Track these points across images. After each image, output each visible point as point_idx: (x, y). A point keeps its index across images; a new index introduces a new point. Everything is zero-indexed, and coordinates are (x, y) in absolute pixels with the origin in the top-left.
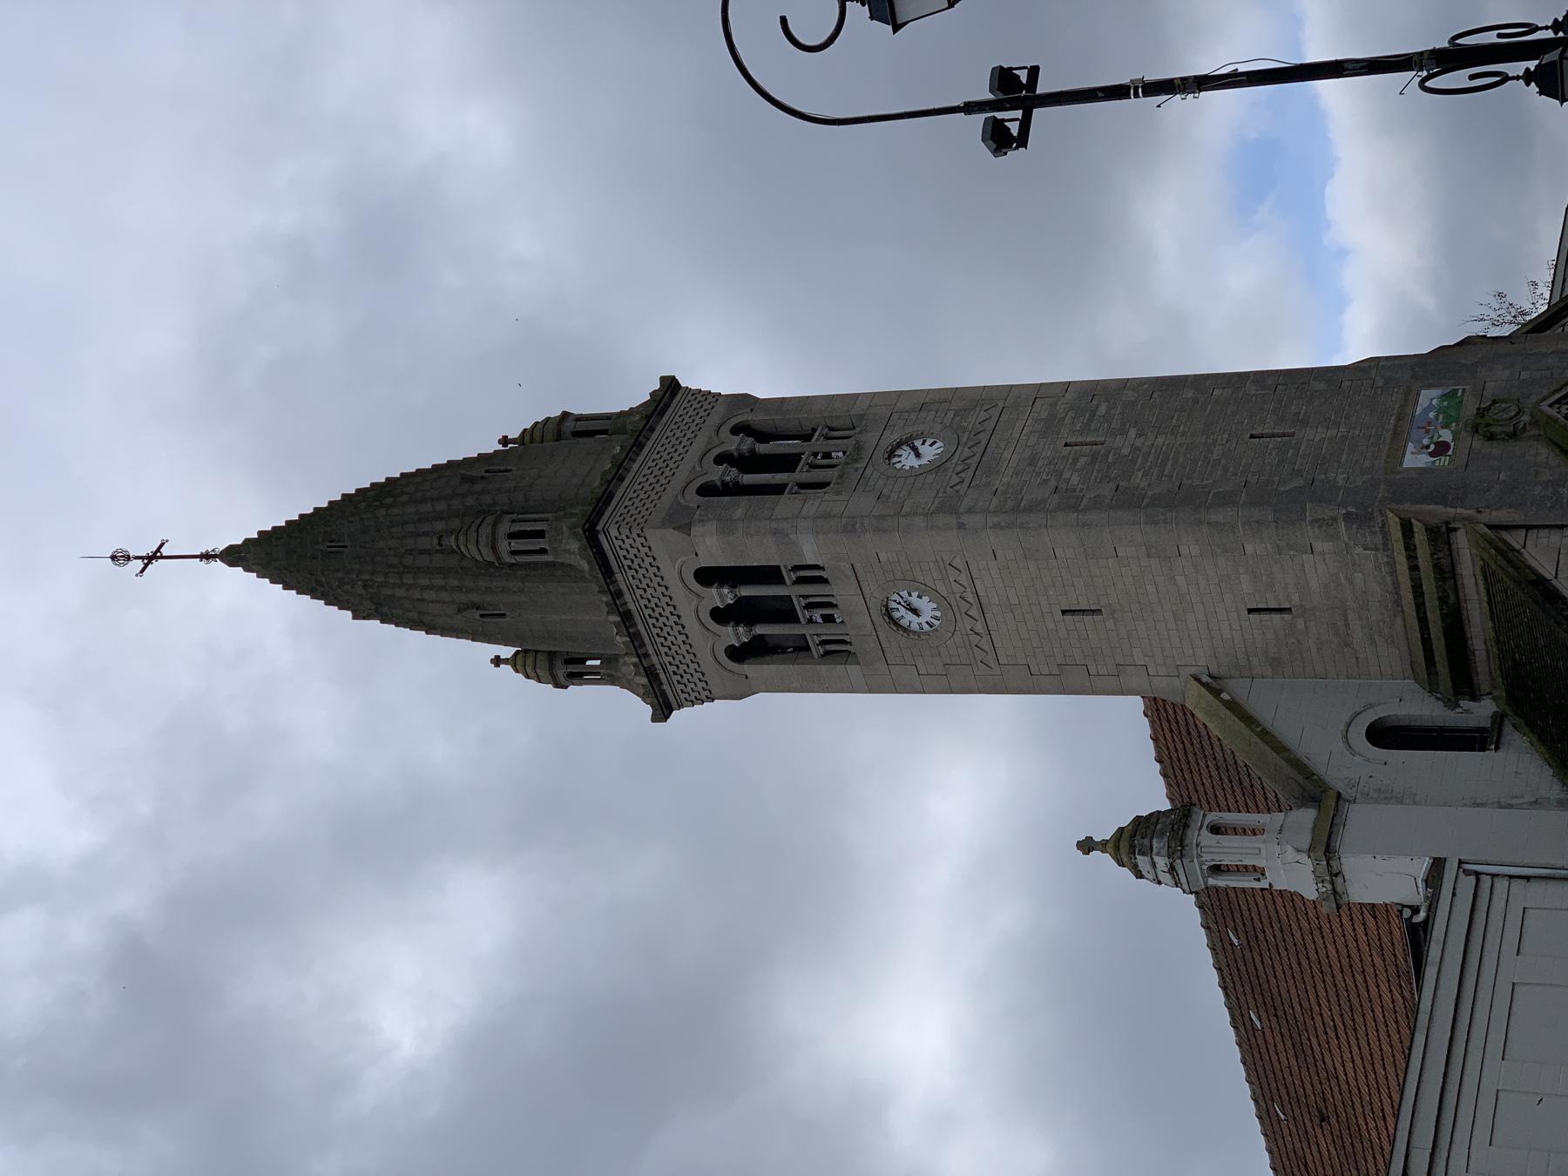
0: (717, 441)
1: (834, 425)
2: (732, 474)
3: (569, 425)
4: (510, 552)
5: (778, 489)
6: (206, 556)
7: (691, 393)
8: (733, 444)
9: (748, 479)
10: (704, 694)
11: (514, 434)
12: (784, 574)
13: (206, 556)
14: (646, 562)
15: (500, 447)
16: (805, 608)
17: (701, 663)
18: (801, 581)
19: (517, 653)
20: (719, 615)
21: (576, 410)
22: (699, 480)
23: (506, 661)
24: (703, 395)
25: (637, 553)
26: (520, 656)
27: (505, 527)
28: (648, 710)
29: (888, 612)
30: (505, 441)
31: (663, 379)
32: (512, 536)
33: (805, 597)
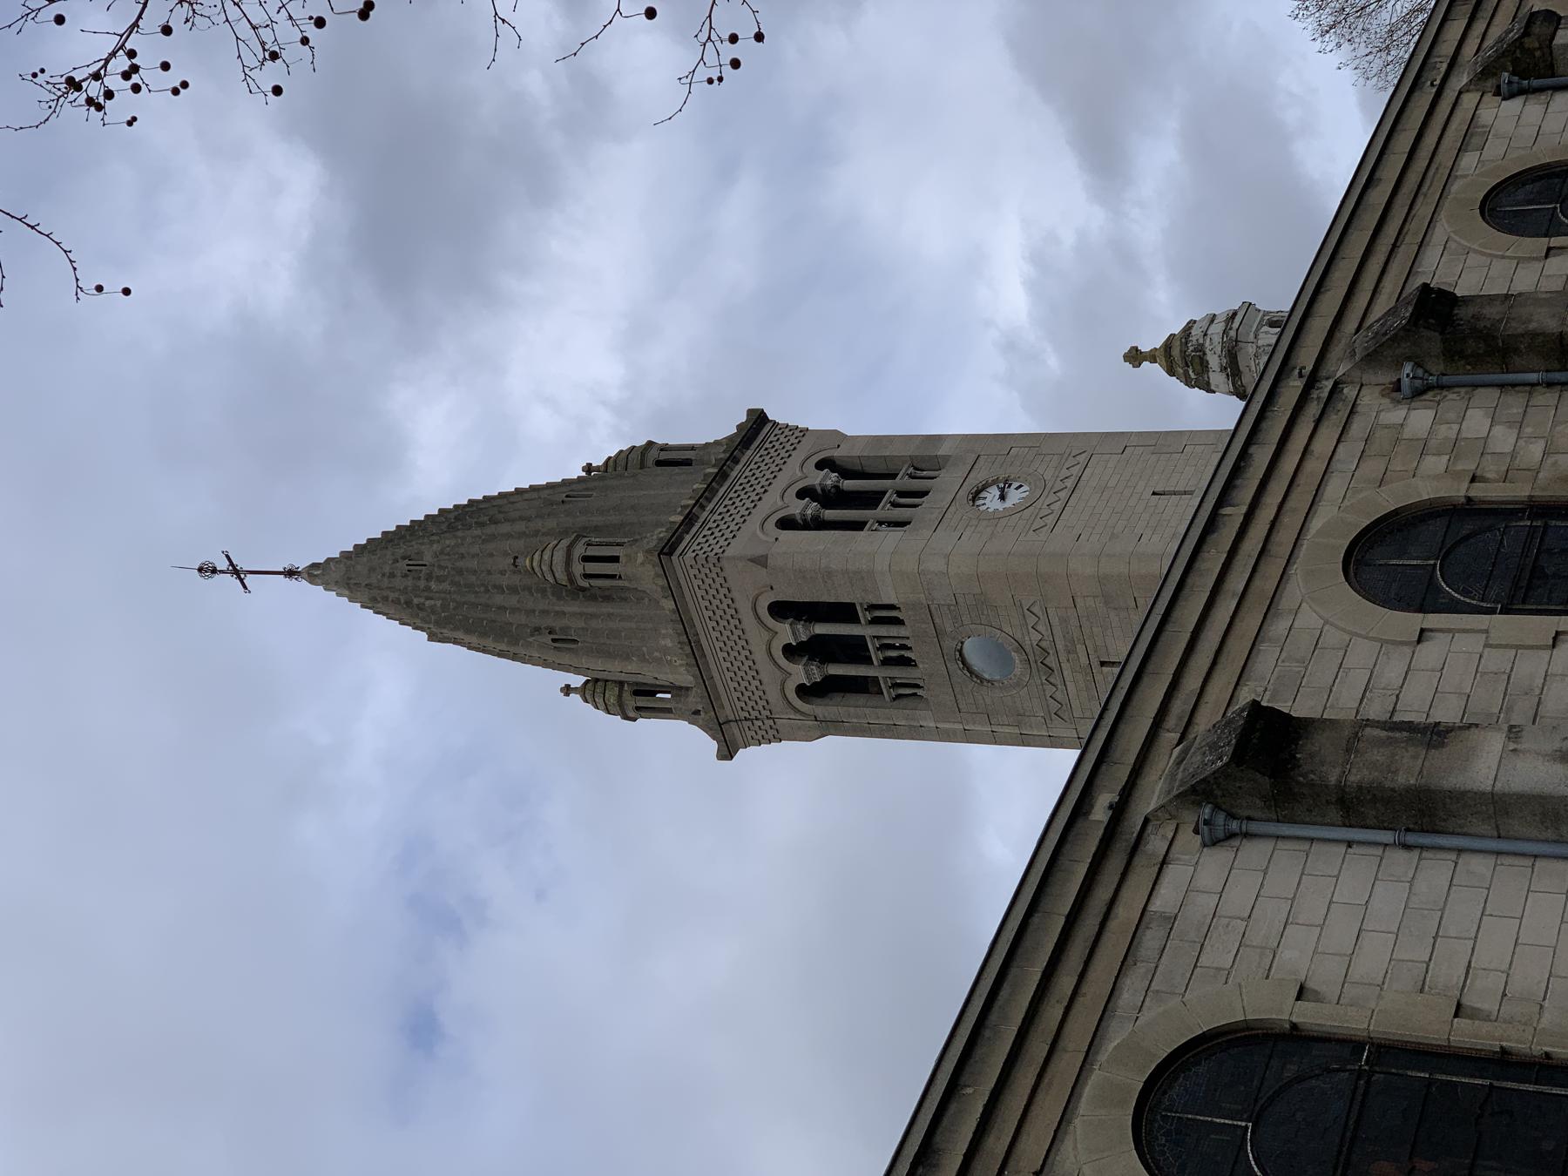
0: (780, 503)
1: (919, 466)
2: (812, 508)
3: (653, 455)
4: (584, 575)
5: (858, 526)
6: (290, 573)
7: (779, 426)
8: (819, 479)
9: (830, 514)
10: (771, 732)
11: (598, 462)
12: (860, 614)
13: (290, 573)
14: (769, 733)
15: (584, 474)
16: (878, 649)
17: (750, 641)
18: (886, 662)
19: (587, 682)
20: (789, 651)
21: (660, 441)
22: (783, 511)
23: (575, 690)
24: (790, 430)
25: (755, 705)
26: (590, 685)
27: (580, 550)
28: (713, 746)
30: (588, 468)
31: (750, 412)
32: (586, 559)
33: (878, 638)
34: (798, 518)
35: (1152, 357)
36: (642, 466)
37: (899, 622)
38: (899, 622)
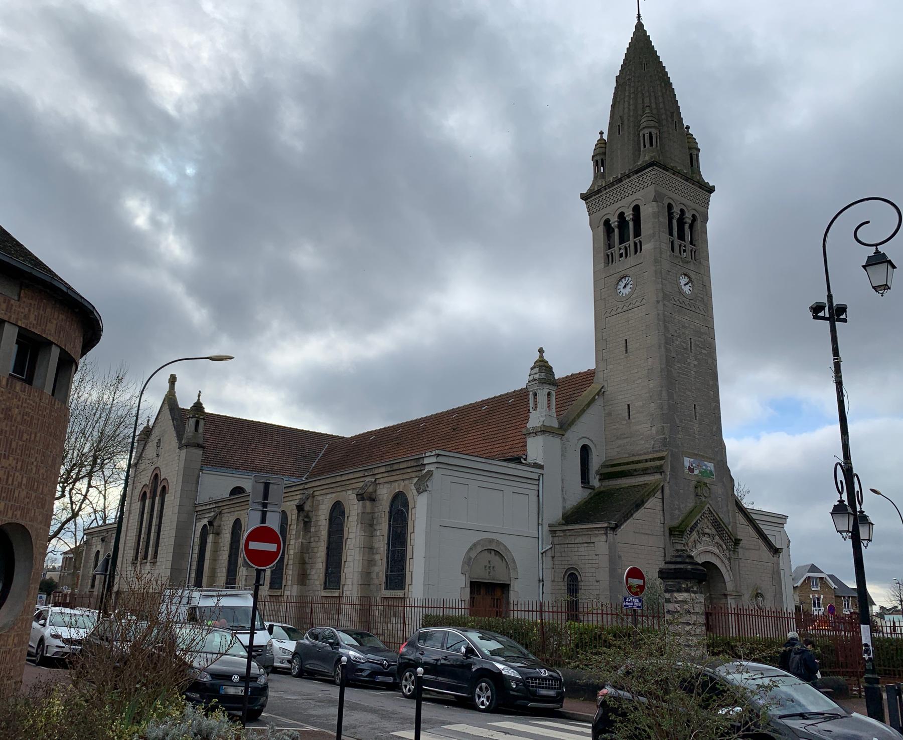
3: (694, 152)
5: (671, 234)
6: (639, 16)
9: (675, 222)
13: (639, 16)
15: (685, 126)
18: (636, 244)
23: (602, 136)
26: (604, 142)
27: (653, 131)
29: (624, 277)
31: (714, 187)
32: (650, 134)
33: (629, 246)
34: (673, 211)
35: (541, 356)
36: (690, 148)
37: (636, 252)
38: (636, 252)
